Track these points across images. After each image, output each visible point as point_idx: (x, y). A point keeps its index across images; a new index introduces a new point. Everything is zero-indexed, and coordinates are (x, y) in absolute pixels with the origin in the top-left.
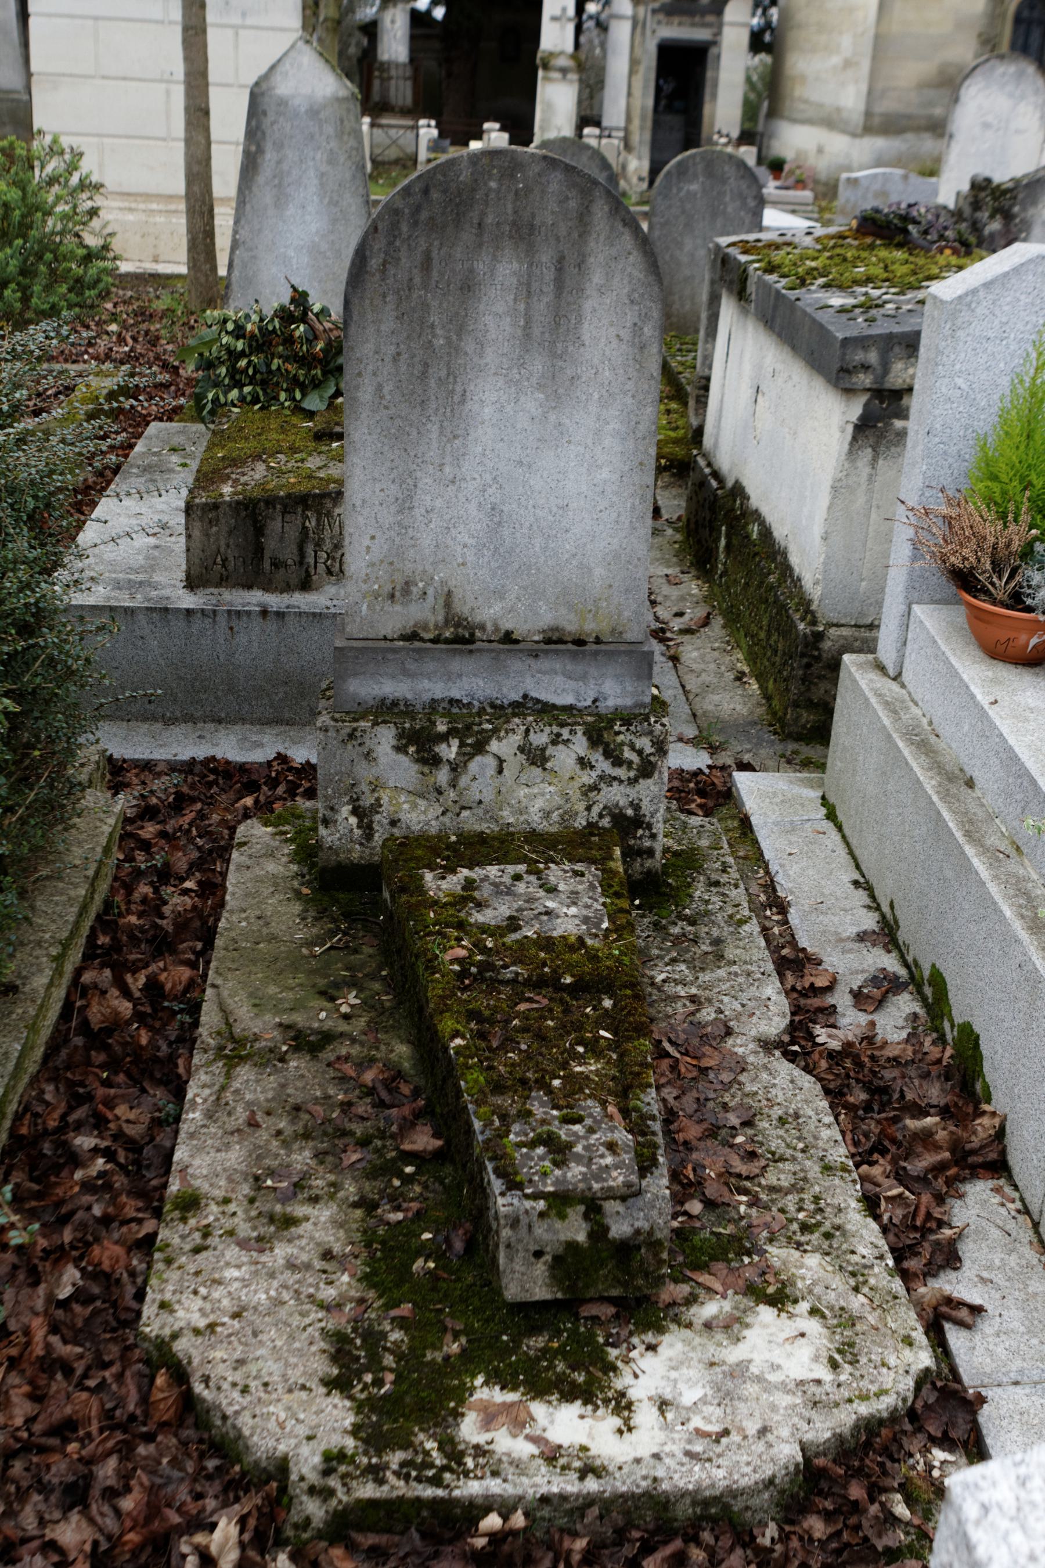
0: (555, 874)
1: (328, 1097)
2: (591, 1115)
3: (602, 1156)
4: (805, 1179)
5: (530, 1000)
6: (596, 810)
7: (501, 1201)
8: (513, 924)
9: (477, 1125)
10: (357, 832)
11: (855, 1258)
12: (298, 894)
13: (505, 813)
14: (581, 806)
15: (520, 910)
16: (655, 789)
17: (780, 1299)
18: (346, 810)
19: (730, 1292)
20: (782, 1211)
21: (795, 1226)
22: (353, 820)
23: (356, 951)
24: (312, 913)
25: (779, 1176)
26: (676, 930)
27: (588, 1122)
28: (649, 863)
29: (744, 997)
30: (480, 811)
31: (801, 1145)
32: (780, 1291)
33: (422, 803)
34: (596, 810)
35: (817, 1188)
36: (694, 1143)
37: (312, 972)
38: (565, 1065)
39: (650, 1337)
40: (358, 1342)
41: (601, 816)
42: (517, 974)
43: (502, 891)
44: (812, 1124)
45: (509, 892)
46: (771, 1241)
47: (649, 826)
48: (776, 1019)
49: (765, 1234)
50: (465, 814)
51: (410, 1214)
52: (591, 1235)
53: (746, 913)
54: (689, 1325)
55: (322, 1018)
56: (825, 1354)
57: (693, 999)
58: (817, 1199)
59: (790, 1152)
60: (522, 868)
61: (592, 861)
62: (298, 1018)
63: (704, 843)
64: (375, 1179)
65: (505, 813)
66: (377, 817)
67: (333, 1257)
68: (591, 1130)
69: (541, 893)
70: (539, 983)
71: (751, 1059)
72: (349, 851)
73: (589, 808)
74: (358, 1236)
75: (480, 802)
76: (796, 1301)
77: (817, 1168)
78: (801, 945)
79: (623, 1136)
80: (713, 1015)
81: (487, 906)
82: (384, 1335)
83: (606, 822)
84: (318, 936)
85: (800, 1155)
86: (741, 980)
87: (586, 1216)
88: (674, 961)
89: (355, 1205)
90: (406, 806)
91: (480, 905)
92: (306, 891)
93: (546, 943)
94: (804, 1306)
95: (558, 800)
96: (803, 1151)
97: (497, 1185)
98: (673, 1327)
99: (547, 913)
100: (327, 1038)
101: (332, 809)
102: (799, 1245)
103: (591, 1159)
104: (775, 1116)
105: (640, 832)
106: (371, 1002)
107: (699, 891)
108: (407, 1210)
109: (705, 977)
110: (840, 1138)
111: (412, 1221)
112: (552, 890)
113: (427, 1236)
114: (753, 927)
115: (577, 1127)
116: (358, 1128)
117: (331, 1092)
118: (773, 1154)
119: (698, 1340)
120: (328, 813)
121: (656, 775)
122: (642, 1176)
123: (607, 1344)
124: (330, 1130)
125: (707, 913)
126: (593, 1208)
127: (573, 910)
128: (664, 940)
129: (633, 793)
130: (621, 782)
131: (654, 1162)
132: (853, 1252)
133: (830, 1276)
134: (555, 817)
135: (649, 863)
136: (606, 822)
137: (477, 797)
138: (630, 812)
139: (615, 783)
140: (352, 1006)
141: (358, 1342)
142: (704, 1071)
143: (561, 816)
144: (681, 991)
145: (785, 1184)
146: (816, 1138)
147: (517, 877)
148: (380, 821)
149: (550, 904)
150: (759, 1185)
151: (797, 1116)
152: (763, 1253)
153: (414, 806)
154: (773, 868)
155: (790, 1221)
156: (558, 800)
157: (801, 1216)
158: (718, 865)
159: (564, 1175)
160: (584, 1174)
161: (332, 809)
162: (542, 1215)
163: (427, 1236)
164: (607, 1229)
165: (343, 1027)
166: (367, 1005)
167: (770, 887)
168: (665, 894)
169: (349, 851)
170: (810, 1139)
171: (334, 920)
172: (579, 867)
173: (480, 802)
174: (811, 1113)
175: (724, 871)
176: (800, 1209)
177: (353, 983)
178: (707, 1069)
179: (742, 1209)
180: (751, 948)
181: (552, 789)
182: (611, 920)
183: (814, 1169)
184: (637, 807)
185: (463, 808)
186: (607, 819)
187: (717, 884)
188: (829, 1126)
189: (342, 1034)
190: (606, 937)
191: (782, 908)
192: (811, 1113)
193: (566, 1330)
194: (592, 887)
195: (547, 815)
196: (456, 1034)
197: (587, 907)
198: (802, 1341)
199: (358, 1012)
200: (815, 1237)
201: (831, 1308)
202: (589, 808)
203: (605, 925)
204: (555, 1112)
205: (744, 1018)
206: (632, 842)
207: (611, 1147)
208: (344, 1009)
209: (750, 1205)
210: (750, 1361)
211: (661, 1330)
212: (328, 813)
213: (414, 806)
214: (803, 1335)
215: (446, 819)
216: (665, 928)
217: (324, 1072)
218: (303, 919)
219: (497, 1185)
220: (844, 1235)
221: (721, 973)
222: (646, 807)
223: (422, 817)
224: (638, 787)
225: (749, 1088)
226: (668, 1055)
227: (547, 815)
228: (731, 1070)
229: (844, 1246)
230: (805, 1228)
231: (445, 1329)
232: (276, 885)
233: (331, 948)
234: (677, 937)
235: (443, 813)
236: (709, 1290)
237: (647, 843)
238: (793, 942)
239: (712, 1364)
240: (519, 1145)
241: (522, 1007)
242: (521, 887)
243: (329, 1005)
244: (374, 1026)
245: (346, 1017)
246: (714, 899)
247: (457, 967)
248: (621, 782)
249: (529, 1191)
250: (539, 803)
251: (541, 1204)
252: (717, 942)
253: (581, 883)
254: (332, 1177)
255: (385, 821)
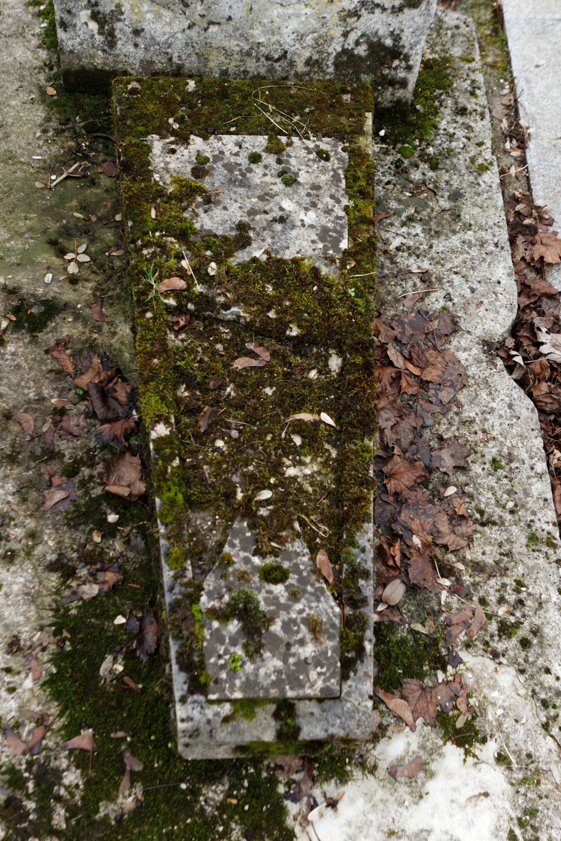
0: (299, 151)
1: (41, 399)
2: (296, 569)
3: (302, 642)
4: (509, 554)
5: (251, 354)
6: (353, 37)
7: (181, 711)
8: (242, 236)
9: (167, 574)
10: (99, 39)
11: (548, 680)
12: (42, 92)
13: (256, 32)
14: (337, 32)
15: (252, 212)
16: (419, 20)
17: (466, 737)
18: (84, 15)
19: (420, 721)
20: (483, 602)
21: (493, 627)
22: (93, 26)
23: (93, 183)
24: (54, 124)
25: (484, 551)
26: (416, 175)
27: (293, 579)
28: (400, 93)
29: (474, 275)
30: (229, 28)
31: (510, 505)
32: (469, 725)
33: (167, 15)
34: (353, 37)
35: (520, 569)
36: (406, 493)
37: (46, 211)
38: (276, 468)
39: (331, 788)
40: (31, 785)
41: (357, 43)
42: (239, 317)
43: (239, 179)
44: (525, 472)
45: (244, 183)
46: (468, 646)
47: (407, 58)
48: (503, 312)
49: (462, 637)
50: (213, 29)
51: (106, 588)
52: (280, 735)
53: (488, 155)
54: (373, 770)
55: (45, 283)
56: (506, 826)
57: (425, 277)
58: (520, 584)
59: (498, 511)
60: (262, 140)
61: (339, 135)
62: (22, 279)
63: (457, 51)
64: (75, 527)
65: (256, 32)
66: (119, 25)
67: (20, 649)
68: (294, 596)
69: (279, 187)
70: (263, 331)
71: (473, 370)
72: (92, 57)
73: (345, 35)
74: (48, 617)
75: (230, 18)
76: (484, 741)
77: (523, 540)
78: (539, 202)
79: (329, 608)
80: (442, 303)
81: (217, 203)
82: (58, 774)
83: (362, 51)
84: (56, 158)
85: (508, 517)
86: (474, 252)
87: (276, 715)
88: (410, 219)
89: (52, 567)
90: (149, 16)
91: (209, 201)
92: (51, 91)
93: (278, 270)
94: (491, 749)
95: (314, 23)
96: (512, 512)
97: (179, 682)
98: (357, 773)
99: (282, 220)
100: (52, 309)
101: (69, 12)
102: (495, 655)
103: (289, 645)
104: (489, 458)
105: (396, 63)
106: (100, 259)
107: (444, 122)
108: (104, 582)
109: (440, 245)
110: (549, 495)
111: (108, 595)
112: (290, 180)
113: (120, 620)
114: (491, 178)
115: (279, 589)
116: (66, 447)
117: (46, 392)
118: (482, 513)
119: (380, 794)
120: (66, 16)
121: (423, 6)
122: (345, 677)
123: (287, 796)
124: (38, 451)
125: (450, 153)
126: (285, 709)
127: (311, 217)
128: (404, 187)
129: (395, 22)
130: (384, 9)
131: (360, 650)
132: (548, 671)
133: (521, 701)
134: (309, 40)
135: (400, 93)
136: (362, 51)
137: (227, 13)
138: (389, 42)
139: (377, 11)
140: (80, 265)
141: (31, 785)
142: (424, 384)
143: (316, 40)
144: (414, 265)
145: (490, 560)
146: (527, 493)
147: (255, 158)
148: (122, 28)
149: (288, 205)
150: (463, 560)
151: (510, 458)
152: (457, 661)
153: (159, 16)
154: (520, 84)
155: (489, 617)
156: (314, 23)
157: (502, 611)
158: (466, 85)
159: (256, 673)
160: (278, 672)
161: (69, 12)
162: (226, 720)
163: (120, 620)
164: (298, 730)
165: (68, 295)
166: (98, 264)
167: (513, 110)
168: (411, 124)
169: (92, 57)
170: (521, 495)
171: (76, 136)
172: (325, 144)
173: (230, 18)
174: (525, 456)
175: (473, 94)
176: (501, 600)
177: (86, 231)
178: (428, 382)
179: (444, 595)
180: (488, 213)
181: (308, 11)
182: (352, 235)
183: (520, 544)
184: (396, 38)
185: (211, 23)
186: (364, 47)
187: (462, 111)
188: (540, 476)
189: (66, 305)
190: (343, 265)
191: (520, 138)
192: (525, 456)
193: (247, 776)
194: (336, 178)
195: (301, 37)
196: (160, 418)
197: (328, 212)
198: (485, 802)
199: (86, 273)
200: (510, 644)
201: (518, 753)
202: (345, 35)
203: (344, 245)
204: (256, 560)
205: (472, 309)
206: (386, 72)
207: (315, 627)
208: (72, 269)
209: (452, 591)
210: (429, 832)
211: (343, 778)
212: (66, 16)
213: (159, 16)
214: (486, 795)
215: (193, 33)
216: (405, 171)
217: (42, 362)
218: (45, 131)
219: (179, 682)
220: (541, 643)
221: (455, 241)
222: (407, 39)
223: (167, 29)
224: (401, 16)
225: (469, 412)
226: (391, 364)
227: (301, 37)
228: (452, 386)
229: (540, 662)
230: (505, 630)
231: (121, 771)
232: (22, 78)
233: (67, 178)
234: (417, 187)
235: (190, 27)
236: (399, 719)
237: (401, 74)
238: (528, 198)
239: (391, 833)
240: (214, 613)
241: (240, 363)
242: (257, 175)
243: (57, 261)
244: (100, 297)
245: (73, 280)
246: (460, 133)
247: (172, 302)
248: (384, 9)
249: (213, 697)
250: (293, 24)
251: (227, 709)
252: (456, 196)
253: (324, 171)
254: (31, 523)
255: (128, 30)
